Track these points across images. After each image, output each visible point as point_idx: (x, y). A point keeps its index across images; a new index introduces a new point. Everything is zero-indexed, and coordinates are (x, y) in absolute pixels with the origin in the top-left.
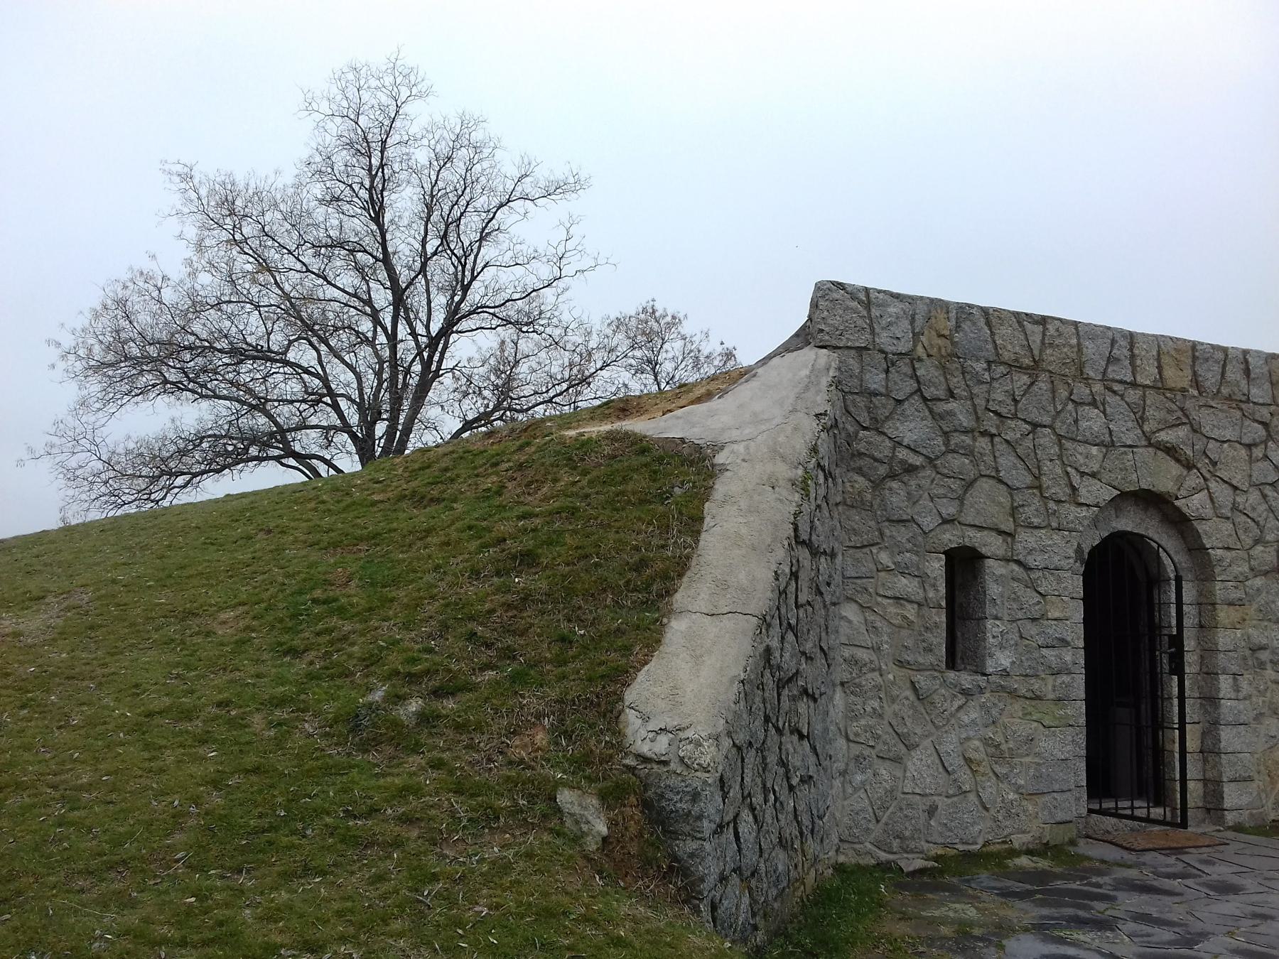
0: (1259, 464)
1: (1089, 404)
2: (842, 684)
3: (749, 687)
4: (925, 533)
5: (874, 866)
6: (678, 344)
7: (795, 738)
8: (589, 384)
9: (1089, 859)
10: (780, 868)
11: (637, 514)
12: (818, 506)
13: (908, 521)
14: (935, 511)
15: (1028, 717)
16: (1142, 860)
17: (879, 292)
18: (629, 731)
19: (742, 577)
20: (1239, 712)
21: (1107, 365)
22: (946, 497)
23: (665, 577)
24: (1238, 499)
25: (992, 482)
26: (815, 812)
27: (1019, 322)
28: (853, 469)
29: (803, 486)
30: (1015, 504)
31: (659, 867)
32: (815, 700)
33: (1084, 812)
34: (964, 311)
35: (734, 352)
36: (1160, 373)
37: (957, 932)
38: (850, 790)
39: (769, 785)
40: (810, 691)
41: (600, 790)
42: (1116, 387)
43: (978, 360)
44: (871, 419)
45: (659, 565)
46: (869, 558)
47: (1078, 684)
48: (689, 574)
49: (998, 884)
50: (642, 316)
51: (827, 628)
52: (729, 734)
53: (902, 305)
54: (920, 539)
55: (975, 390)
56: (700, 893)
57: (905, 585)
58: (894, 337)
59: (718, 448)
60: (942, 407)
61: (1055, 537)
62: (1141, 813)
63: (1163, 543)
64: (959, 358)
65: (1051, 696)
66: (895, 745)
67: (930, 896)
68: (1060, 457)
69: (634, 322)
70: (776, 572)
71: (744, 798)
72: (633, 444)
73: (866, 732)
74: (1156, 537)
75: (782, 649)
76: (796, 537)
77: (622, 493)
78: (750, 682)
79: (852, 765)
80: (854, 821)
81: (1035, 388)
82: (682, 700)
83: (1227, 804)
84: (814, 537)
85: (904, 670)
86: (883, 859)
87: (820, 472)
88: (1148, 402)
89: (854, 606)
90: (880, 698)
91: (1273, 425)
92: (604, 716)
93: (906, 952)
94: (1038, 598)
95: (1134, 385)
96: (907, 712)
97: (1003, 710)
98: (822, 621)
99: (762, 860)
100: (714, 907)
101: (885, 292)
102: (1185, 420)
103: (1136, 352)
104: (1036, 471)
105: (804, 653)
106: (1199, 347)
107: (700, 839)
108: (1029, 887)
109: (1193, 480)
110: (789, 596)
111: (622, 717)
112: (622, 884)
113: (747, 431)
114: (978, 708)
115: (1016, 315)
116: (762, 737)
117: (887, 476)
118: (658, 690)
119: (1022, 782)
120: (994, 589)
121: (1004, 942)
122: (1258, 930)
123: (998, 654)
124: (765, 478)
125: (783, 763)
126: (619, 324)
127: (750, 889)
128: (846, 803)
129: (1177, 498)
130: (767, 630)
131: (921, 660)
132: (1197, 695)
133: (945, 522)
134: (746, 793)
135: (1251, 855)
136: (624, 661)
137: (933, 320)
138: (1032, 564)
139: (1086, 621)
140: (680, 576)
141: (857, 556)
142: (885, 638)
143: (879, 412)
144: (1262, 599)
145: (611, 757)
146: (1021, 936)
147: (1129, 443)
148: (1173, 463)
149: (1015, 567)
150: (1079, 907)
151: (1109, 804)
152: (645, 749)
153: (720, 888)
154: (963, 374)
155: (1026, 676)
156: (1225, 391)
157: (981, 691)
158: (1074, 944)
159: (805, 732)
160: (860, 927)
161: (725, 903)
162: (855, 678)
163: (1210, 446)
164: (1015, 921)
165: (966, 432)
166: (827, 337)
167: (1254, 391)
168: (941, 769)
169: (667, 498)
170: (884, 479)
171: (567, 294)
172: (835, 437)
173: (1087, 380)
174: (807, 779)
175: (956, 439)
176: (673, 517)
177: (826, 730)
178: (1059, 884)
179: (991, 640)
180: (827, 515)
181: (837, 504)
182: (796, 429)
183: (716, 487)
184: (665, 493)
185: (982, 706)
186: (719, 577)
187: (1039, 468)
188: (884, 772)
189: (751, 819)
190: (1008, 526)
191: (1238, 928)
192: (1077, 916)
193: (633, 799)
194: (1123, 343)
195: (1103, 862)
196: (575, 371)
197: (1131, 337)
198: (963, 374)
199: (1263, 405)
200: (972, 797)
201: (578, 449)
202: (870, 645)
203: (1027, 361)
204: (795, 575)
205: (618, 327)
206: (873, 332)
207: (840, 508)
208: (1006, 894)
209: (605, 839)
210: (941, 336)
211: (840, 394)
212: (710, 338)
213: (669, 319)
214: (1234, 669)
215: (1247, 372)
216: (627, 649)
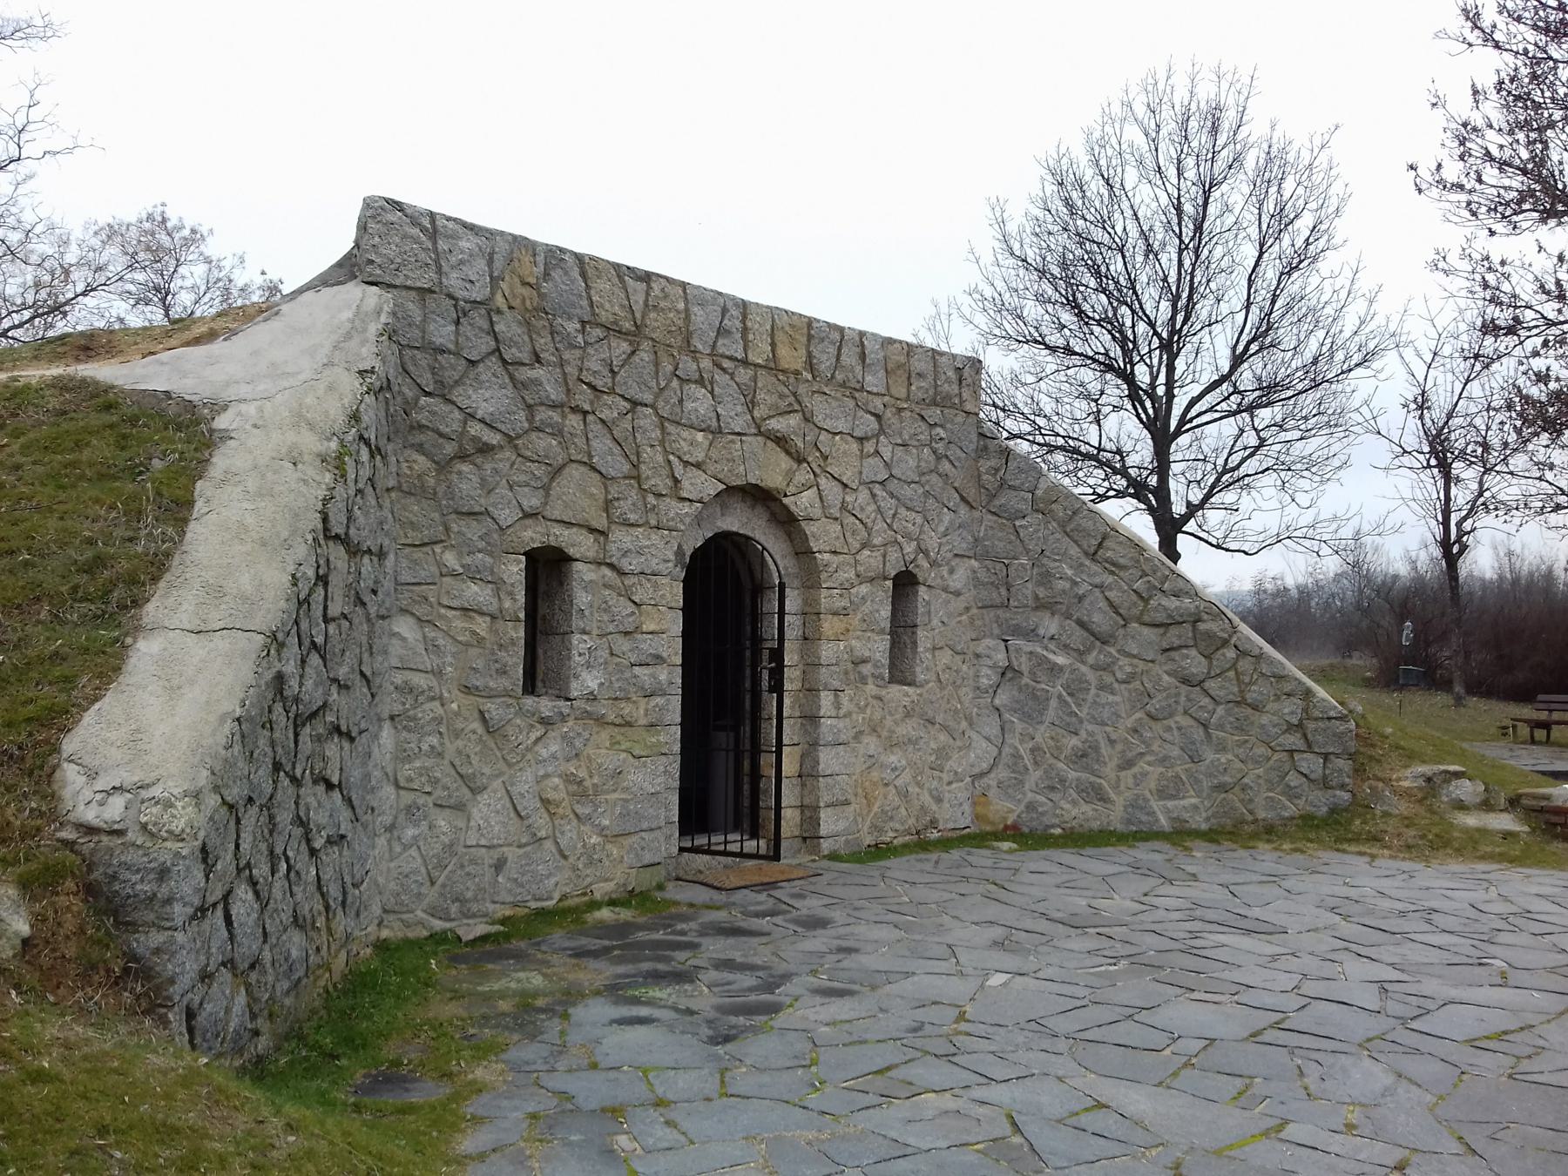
0: (870, 460)
1: (696, 382)
2: (392, 718)
3: (246, 728)
4: (501, 529)
5: (426, 939)
6: (200, 270)
7: (321, 788)
8: (65, 314)
9: (676, 903)
10: (295, 953)
11: (94, 493)
12: (359, 491)
13: (481, 513)
14: (514, 502)
15: (617, 747)
16: (732, 899)
17: (449, 219)
18: (67, 793)
19: (245, 582)
20: (839, 731)
21: (716, 337)
22: (527, 485)
23: (132, 580)
24: (848, 499)
25: (583, 469)
26: (347, 879)
27: (619, 276)
28: (412, 445)
29: (337, 464)
30: (610, 497)
31: (108, 971)
32: (352, 740)
33: (675, 850)
34: (555, 256)
35: (281, 287)
36: (773, 351)
37: (517, 1006)
38: (398, 849)
39: (279, 850)
40: (344, 728)
41: (20, 875)
42: (726, 364)
43: (570, 318)
44: (436, 382)
45: (124, 565)
46: (431, 559)
47: (673, 708)
48: (167, 576)
49: (573, 944)
50: (147, 225)
51: (371, 648)
52: (216, 789)
53: (477, 240)
54: (495, 536)
55: (567, 355)
56: (170, 998)
57: (476, 593)
58: (469, 281)
59: (219, 407)
60: (525, 374)
61: (653, 537)
62: (734, 848)
63: (766, 545)
64: (547, 313)
65: (643, 721)
66: (457, 789)
67: (490, 966)
68: (662, 442)
69: (134, 232)
70: (293, 576)
71: (239, 870)
72: (93, 396)
73: (421, 775)
74: (762, 540)
75: (302, 676)
76: (326, 529)
77: (73, 464)
78: (250, 719)
79: (402, 817)
80: (402, 885)
81: (636, 359)
82: (147, 747)
83: (823, 832)
84: (352, 531)
85: (471, 697)
86: (438, 929)
87: (363, 446)
88: (760, 385)
89: (411, 620)
90: (440, 733)
91: (885, 417)
92: (31, 774)
93: (452, 1038)
94: (631, 608)
95: (745, 362)
96: (473, 749)
97: (587, 740)
98: (364, 639)
99: (267, 947)
100: (190, 1015)
101: (455, 220)
102: (797, 407)
103: (749, 324)
104: (634, 458)
105: (335, 680)
106: (815, 325)
107: (169, 929)
108: (606, 943)
109: (803, 475)
110: (313, 606)
111: (57, 774)
112: (52, 999)
113: (261, 387)
114: (559, 740)
115: (617, 267)
116: (270, 790)
117: (455, 457)
118: (113, 735)
119: (607, 822)
120: (582, 598)
121: (571, 1011)
122: (840, 965)
123: (584, 674)
124: (284, 451)
125: (300, 822)
126: (112, 233)
127: (248, 986)
128: (392, 865)
129: (786, 496)
130: (279, 652)
131: (492, 684)
132: (798, 714)
133: (527, 516)
134: (243, 863)
135: (844, 885)
136: (64, 697)
137: (516, 264)
138: (627, 568)
139: (686, 635)
140: (155, 579)
141: (415, 556)
142: (449, 659)
143: (446, 374)
144: (867, 607)
145: (38, 830)
146: (590, 1002)
147: (738, 430)
148: (783, 455)
149: (607, 572)
150: (659, 959)
151: (701, 840)
152: (90, 815)
153: (201, 989)
154: (552, 334)
155: (616, 699)
156: (839, 377)
157: (563, 718)
158: (650, 1003)
159: (335, 780)
160: (400, 1014)
161: (208, 1007)
162: (408, 710)
163: (822, 438)
164: (586, 984)
165: (554, 406)
166: (378, 272)
167: (868, 378)
168: (512, 815)
169: (141, 473)
170: (451, 459)
171: (30, 185)
172: (387, 403)
173: (694, 353)
174: (338, 840)
175: (543, 414)
176: (148, 499)
177: (367, 776)
178: (642, 936)
179: (577, 658)
180: (374, 502)
181: (388, 490)
182: (331, 388)
183: (214, 460)
184: (137, 466)
185: (564, 737)
186: (211, 581)
187: (638, 455)
188: (443, 823)
189: (250, 896)
190: (600, 522)
191: (822, 965)
192: (656, 971)
193: (70, 884)
194: (735, 312)
195: (691, 905)
196: (43, 294)
197: (744, 306)
198: (552, 334)
199: (877, 394)
200: (549, 845)
201: (8, 399)
202: (429, 669)
203: (627, 326)
204: (323, 580)
205: (109, 237)
206: (439, 271)
207: (393, 495)
208: (580, 954)
209: (26, 942)
210: (525, 284)
211: (395, 347)
212: (245, 264)
213: (186, 232)
214: (836, 684)
215: (863, 357)
216: (68, 681)
